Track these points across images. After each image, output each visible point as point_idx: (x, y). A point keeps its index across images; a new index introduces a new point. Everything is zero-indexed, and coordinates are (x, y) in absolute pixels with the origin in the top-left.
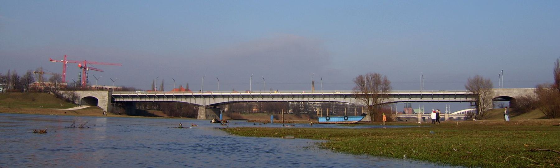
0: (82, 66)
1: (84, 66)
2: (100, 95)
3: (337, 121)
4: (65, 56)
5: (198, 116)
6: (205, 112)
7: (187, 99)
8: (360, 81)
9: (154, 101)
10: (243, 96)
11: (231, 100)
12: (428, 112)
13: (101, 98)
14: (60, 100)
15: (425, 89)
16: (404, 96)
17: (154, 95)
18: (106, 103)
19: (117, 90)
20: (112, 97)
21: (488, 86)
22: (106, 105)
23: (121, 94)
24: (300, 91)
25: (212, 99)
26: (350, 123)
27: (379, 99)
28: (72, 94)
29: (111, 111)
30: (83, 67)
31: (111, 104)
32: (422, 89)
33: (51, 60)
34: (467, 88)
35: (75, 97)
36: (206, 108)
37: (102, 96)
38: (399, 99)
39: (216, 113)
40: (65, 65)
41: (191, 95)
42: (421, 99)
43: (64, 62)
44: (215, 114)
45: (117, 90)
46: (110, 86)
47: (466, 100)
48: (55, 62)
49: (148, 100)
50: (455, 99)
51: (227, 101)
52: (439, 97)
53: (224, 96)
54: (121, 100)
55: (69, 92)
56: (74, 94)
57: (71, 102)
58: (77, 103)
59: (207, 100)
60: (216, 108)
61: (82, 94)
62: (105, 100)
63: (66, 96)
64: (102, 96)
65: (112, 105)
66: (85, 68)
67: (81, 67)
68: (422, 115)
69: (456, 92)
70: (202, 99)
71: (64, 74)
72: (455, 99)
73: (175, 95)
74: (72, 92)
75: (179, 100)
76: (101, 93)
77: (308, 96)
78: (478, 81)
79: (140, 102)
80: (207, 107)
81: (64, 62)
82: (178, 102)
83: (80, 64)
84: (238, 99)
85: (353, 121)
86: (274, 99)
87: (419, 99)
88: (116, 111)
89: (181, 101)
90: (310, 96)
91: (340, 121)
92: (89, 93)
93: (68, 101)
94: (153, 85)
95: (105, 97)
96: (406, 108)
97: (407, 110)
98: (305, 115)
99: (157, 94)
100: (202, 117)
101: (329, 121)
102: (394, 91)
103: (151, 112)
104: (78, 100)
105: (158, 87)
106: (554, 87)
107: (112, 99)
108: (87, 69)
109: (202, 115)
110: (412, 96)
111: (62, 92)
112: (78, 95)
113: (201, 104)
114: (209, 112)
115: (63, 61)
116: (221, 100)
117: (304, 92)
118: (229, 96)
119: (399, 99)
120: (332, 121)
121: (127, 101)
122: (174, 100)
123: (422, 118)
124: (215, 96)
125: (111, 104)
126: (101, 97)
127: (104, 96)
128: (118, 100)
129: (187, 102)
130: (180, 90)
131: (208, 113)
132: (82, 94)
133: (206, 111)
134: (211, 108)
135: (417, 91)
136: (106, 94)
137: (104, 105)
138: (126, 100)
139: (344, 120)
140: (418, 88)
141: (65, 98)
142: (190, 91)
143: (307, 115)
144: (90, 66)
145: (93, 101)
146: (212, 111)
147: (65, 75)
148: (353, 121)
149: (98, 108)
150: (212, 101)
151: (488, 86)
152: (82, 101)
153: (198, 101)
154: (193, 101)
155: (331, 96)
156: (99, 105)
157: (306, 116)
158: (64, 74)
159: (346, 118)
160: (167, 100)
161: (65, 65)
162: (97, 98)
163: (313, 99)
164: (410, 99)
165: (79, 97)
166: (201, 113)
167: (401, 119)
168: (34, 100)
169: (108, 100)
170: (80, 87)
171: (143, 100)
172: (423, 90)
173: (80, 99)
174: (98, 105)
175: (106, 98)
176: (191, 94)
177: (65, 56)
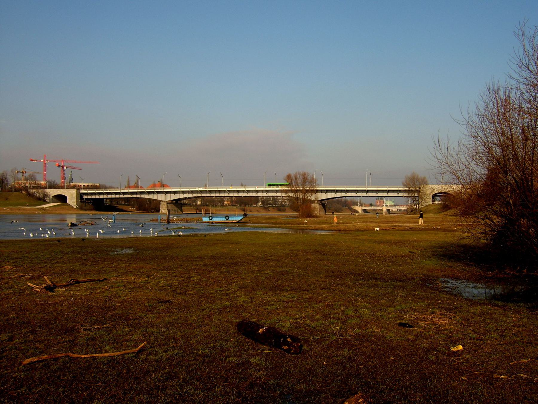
0: (60, 165)
1: (62, 164)
2: (69, 193)
3: (220, 220)
4: (45, 156)
5: (160, 211)
6: (166, 207)
7: (158, 195)
8: (289, 177)
9: (120, 198)
10: (201, 192)
11: (190, 195)
12: (398, 204)
13: (69, 196)
14: (32, 198)
15: (373, 184)
16: (351, 192)
17: (162, 191)
18: (75, 200)
19: (88, 187)
20: (80, 194)
21: (424, 182)
22: (74, 202)
23: (89, 192)
24: (253, 187)
25: (323, 193)
26: (231, 222)
27: (307, 195)
28: (43, 193)
29: (81, 208)
30: (61, 166)
31: (80, 201)
32: (367, 185)
33: (32, 160)
34: (404, 185)
35: (45, 195)
36: (167, 203)
37: (71, 194)
38: (346, 194)
39: (178, 207)
40: (45, 165)
41: (153, 192)
42: (367, 194)
43: (44, 161)
44: (176, 209)
45: (88, 187)
46: (87, 183)
47: (398, 195)
48: (35, 161)
49: (122, 196)
50: (398, 194)
51: (187, 197)
52: (383, 193)
53: (184, 192)
54: (89, 197)
55: (40, 190)
56: (44, 193)
57: (43, 200)
58: (48, 200)
59: (169, 195)
60: (178, 204)
61: (53, 192)
62: (74, 197)
63: (38, 195)
64: (71, 194)
65: (80, 202)
66: (63, 167)
67: (59, 166)
68: (387, 207)
69: (378, 188)
70: (164, 195)
71: (45, 173)
72: (398, 194)
73: (155, 191)
74: (42, 191)
75: (143, 196)
76: (70, 191)
77: (320, 191)
78: (414, 178)
79: (256, 196)
80: (168, 203)
81: (44, 161)
82: (142, 198)
83: (57, 164)
84: (233, 194)
85: (234, 220)
86: (258, 194)
87: (365, 194)
88: (85, 208)
89: (144, 197)
90: (322, 191)
91: (222, 220)
92: (59, 192)
93: (39, 199)
94: (129, 182)
95: (74, 195)
96: (377, 201)
97: (379, 202)
98: (273, 207)
99: (164, 190)
100: (163, 211)
101: (212, 220)
102: (321, 186)
103: (120, 207)
104: (49, 197)
105: (132, 184)
106: (485, 184)
107: (80, 196)
108: (65, 168)
109: (163, 210)
110: (379, 191)
111: (34, 190)
112: (49, 193)
113: (163, 200)
114: (173, 208)
115: (43, 160)
116: (181, 196)
117: (257, 188)
118: (188, 192)
119: (346, 194)
120: (214, 220)
121: (95, 197)
122: (138, 196)
123: (363, 210)
124: (175, 192)
125: (80, 201)
126: (70, 195)
127: (73, 194)
128: (85, 197)
129: (154, 198)
130: (154, 186)
131: (170, 208)
132: (53, 192)
133: (167, 206)
134: (172, 203)
135: (362, 186)
136: (74, 191)
137: (73, 202)
138: (93, 197)
139: (225, 220)
140: (363, 184)
141: (36, 197)
142: (169, 187)
143: (275, 208)
144: (68, 165)
145: (62, 199)
146: (174, 206)
147: (45, 174)
148: (234, 220)
149: (67, 205)
150: (172, 197)
151: (424, 182)
152: (53, 198)
153: (160, 197)
154: (155, 197)
155: (363, 191)
156: (68, 202)
157: (274, 209)
158: (45, 173)
159: (211, 218)
160: (131, 197)
161: (45, 165)
162: (66, 196)
163: (266, 194)
164: (356, 194)
165: (50, 195)
166: (162, 208)
167: (367, 211)
168: (7, 199)
169: (77, 197)
170: (52, 186)
171: (118, 196)
172: (368, 186)
173: (51, 197)
174: (67, 203)
175: (75, 195)
176: (144, 191)
177: (45, 156)
